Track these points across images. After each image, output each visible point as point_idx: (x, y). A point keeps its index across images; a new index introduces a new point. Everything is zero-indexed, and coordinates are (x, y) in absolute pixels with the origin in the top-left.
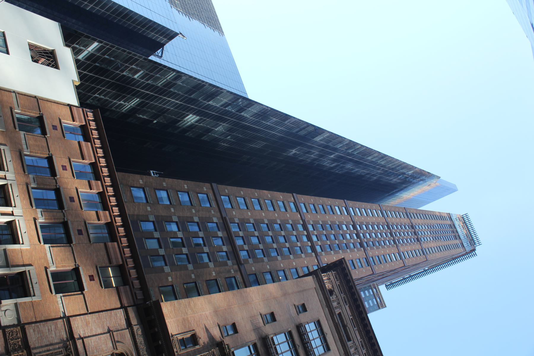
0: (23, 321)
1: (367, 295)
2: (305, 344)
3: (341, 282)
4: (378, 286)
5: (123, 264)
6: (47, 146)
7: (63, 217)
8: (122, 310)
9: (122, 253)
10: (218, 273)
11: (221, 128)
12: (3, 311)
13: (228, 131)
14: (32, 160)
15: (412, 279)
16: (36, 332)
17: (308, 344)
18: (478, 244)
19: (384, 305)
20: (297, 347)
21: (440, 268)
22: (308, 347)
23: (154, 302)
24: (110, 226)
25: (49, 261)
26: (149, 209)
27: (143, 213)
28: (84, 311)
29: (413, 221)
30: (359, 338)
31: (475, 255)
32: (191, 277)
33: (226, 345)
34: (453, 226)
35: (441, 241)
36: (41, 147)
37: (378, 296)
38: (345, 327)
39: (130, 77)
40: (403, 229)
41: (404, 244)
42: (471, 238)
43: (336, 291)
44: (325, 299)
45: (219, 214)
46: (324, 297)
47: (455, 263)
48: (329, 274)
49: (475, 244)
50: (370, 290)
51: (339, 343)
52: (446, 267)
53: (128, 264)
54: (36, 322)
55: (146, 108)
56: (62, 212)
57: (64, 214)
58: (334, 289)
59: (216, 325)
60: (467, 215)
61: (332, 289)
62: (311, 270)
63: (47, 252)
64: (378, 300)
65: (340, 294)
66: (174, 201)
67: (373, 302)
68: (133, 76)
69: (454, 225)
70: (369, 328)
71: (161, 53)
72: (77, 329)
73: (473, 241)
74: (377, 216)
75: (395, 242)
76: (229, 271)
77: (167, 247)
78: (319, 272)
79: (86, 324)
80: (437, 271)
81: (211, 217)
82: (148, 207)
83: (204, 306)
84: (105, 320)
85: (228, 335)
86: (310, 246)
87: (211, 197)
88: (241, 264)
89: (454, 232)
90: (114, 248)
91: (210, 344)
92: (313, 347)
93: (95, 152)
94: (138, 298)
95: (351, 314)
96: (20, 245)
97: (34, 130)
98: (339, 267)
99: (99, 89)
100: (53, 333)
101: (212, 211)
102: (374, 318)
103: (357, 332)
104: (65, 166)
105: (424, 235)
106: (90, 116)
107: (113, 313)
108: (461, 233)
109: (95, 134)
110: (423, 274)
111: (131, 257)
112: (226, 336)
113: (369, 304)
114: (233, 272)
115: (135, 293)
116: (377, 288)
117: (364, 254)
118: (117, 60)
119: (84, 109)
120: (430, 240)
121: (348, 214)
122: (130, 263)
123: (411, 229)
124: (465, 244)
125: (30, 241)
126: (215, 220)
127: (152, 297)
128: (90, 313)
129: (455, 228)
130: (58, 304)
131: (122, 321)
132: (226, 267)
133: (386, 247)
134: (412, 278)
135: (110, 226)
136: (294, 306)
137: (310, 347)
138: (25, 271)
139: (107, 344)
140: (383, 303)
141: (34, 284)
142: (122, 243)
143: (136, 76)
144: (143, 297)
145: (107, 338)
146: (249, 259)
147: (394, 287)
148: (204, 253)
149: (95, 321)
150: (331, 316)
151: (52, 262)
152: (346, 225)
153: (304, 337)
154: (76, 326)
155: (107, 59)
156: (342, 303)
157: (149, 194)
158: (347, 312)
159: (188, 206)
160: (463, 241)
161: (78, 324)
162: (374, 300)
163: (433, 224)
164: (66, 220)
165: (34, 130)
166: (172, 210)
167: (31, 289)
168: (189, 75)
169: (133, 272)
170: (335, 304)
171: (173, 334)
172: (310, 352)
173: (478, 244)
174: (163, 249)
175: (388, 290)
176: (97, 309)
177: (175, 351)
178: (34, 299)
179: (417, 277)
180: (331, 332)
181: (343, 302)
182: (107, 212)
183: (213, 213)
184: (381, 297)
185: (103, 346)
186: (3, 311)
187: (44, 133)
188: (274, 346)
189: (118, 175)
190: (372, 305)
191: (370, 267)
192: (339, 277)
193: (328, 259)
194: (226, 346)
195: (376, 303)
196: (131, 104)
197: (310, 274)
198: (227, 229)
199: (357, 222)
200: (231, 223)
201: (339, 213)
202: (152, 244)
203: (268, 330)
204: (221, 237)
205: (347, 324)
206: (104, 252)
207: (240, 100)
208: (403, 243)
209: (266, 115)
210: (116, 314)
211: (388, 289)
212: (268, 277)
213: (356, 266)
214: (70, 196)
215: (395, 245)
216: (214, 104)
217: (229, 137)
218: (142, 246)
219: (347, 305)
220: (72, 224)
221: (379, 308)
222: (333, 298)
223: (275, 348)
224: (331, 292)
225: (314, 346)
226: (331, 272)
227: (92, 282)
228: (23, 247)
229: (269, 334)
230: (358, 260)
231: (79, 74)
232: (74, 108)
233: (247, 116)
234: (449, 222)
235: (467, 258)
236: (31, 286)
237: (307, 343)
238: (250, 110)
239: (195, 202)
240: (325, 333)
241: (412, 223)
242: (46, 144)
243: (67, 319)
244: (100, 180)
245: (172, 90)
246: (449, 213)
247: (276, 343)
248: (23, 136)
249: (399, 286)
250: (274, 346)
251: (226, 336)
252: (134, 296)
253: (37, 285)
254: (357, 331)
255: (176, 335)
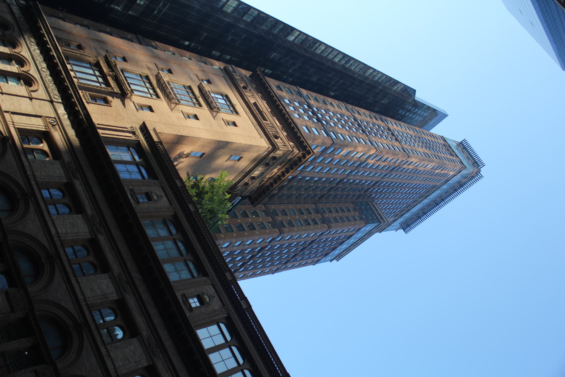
15: (411, 228)
18: (482, 166)
21: (459, 192)
31: (482, 177)
47: (464, 190)
52: (463, 192)
73: (477, 164)
80: (454, 199)
97: (115, 98)
110: (425, 217)
124: (465, 163)
134: (422, 219)
147: (412, 229)
165: (115, 98)
173: (482, 166)
175: (406, 233)
179: (425, 219)
211: (407, 233)
235: (436, 211)
249: (410, 231)
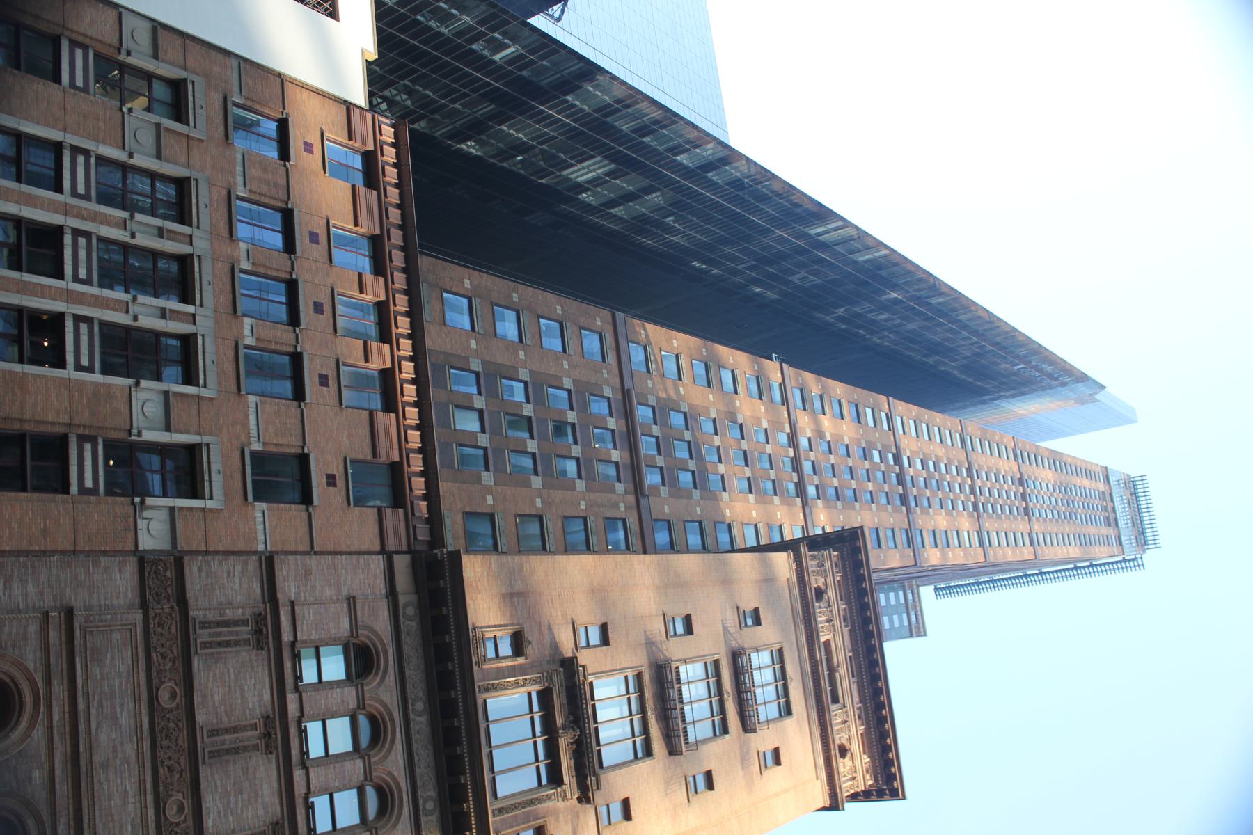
0: (182, 544)
1: (893, 602)
2: (743, 692)
3: (844, 577)
4: (918, 586)
5: (375, 151)
6: (285, 184)
7: (281, 110)
8: (381, 556)
9: (402, 438)
10: (590, 505)
11: (657, 197)
12: (146, 519)
13: (670, 205)
14: (250, 209)
16: (204, 574)
17: (749, 694)
18: (1153, 546)
19: (922, 630)
20: (725, 696)
22: (747, 700)
23: (450, 553)
24: (387, 378)
25: (251, 431)
26: (473, 344)
27: (459, 351)
28: (304, 547)
29: (1024, 469)
30: (856, 698)
32: (533, 503)
33: (581, 666)
34: (1108, 498)
35: (1074, 523)
36: (274, 186)
37: (913, 608)
38: (832, 671)
39: (484, 57)
40: (1000, 482)
41: (994, 515)
42: (1140, 529)
43: (831, 594)
44: (803, 607)
45: (618, 380)
46: (802, 601)
48: (823, 556)
49: (1145, 544)
50: (901, 593)
51: (813, 704)
53: (411, 463)
54: (206, 553)
55: (506, 126)
56: (295, 331)
57: (297, 335)
58: (827, 588)
59: (567, 621)
60: (1144, 478)
61: (823, 587)
62: (787, 537)
63: (250, 413)
64: (913, 618)
65: (837, 600)
66: (528, 336)
67: (901, 620)
68: (492, 55)
69: (1111, 495)
70: (879, 670)
71: (559, 11)
72: (284, 581)
74: (950, 444)
75: (976, 508)
76: (616, 506)
77: (496, 432)
78: (803, 547)
79: (306, 573)
81: (599, 383)
82: (471, 341)
83: (550, 577)
84: (344, 572)
85: (588, 645)
86: (792, 459)
87: (608, 341)
88: (644, 495)
89: (1104, 499)
90: (387, 425)
91: (548, 659)
92: (755, 681)
93: (383, 214)
94: (419, 538)
95: (850, 647)
96: (197, 388)
98: (847, 544)
99: (415, 71)
100: (237, 580)
101: (605, 371)
102: (897, 654)
103: (854, 687)
104: (321, 305)
105: (1038, 491)
106: (388, 134)
107: (362, 561)
108: (1124, 526)
109: (391, 175)
111: (420, 451)
112: (583, 648)
113: (891, 621)
114: (623, 509)
115: (415, 527)
116: (915, 591)
117: (906, 520)
118: (464, 17)
119: (376, 116)
120: (1048, 490)
121: (889, 429)
122: (417, 464)
123: (1017, 484)
125: (219, 383)
126: (607, 391)
127: (447, 531)
128: (315, 553)
129: (1112, 501)
130: (255, 524)
131: (378, 581)
132: (610, 496)
133: (955, 515)
135: (387, 378)
136: (736, 610)
137: (750, 702)
138: (200, 445)
139: (338, 623)
140: (921, 626)
141: (213, 475)
142: (405, 393)
143: (497, 57)
144: (429, 539)
145: (342, 610)
146: (662, 488)
148: (570, 457)
149: (323, 570)
150: (808, 643)
151: (256, 435)
152: (880, 452)
153: (744, 678)
154: (285, 573)
155: (443, 9)
156: (836, 621)
157: (479, 313)
158: (843, 642)
159: (555, 352)
160: (1113, 491)
161: (288, 572)
162: (905, 616)
163: (1067, 484)
164: (299, 350)
166: (522, 355)
167: (207, 484)
168: (611, 74)
169: (419, 485)
170: (821, 619)
171: (478, 624)
172: (743, 674)
173: (1153, 546)
174: (488, 436)
176: (332, 547)
177: (474, 661)
178: (210, 504)
180: (803, 679)
181: (840, 619)
182: (387, 347)
183: (605, 375)
184: (919, 613)
185: (332, 625)
186: (146, 519)
187: (299, 395)
188: (681, 706)
189: (424, 262)
190: (897, 624)
191: (911, 550)
192: (844, 565)
193: (824, 521)
194: (581, 669)
195: (906, 623)
196: (476, 112)
197: (782, 546)
198: (628, 415)
199: (904, 449)
200: (639, 404)
201: (871, 423)
202: (467, 423)
203: (675, 649)
204: (609, 399)
205: (838, 666)
206: (365, 431)
207: (710, 146)
208: (993, 512)
209: (760, 187)
210: (369, 564)
212: (694, 540)
213: (883, 543)
214: (316, 300)
215: (975, 513)
216: (654, 144)
217: (672, 218)
218: (446, 422)
219: (846, 626)
220: (311, 360)
221: (911, 636)
222: (846, 763)
223: (680, 690)
224: (820, 594)
225: (760, 700)
226: (830, 552)
227: (331, 488)
228: (204, 392)
229: (673, 659)
230: (889, 534)
231: (379, 31)
232: (357, 111)
233: (719, 181)
234: (1101, 486)
236: (206, 477)
237: (746, 692)
238: (727, 170)
239: (571, 347)
240: (788, 677)
241: (1021, 474)
242: (285, 181)
243: (268, 564)
244: (403, 506)
245: (568, 98)
246: (1106, 468)
247: (688, 718)
248: (252, 406)
250: (681, 706)
251: (583, 648)
252: (411, 531)
253: (203, 112)
254: (855, 684)
255: (482, 627)
